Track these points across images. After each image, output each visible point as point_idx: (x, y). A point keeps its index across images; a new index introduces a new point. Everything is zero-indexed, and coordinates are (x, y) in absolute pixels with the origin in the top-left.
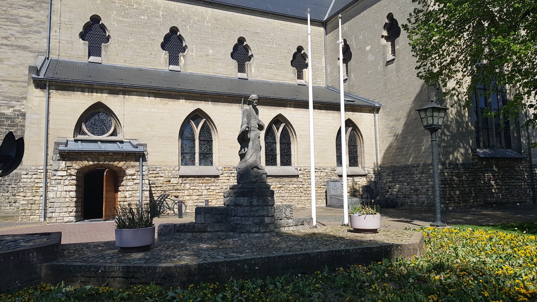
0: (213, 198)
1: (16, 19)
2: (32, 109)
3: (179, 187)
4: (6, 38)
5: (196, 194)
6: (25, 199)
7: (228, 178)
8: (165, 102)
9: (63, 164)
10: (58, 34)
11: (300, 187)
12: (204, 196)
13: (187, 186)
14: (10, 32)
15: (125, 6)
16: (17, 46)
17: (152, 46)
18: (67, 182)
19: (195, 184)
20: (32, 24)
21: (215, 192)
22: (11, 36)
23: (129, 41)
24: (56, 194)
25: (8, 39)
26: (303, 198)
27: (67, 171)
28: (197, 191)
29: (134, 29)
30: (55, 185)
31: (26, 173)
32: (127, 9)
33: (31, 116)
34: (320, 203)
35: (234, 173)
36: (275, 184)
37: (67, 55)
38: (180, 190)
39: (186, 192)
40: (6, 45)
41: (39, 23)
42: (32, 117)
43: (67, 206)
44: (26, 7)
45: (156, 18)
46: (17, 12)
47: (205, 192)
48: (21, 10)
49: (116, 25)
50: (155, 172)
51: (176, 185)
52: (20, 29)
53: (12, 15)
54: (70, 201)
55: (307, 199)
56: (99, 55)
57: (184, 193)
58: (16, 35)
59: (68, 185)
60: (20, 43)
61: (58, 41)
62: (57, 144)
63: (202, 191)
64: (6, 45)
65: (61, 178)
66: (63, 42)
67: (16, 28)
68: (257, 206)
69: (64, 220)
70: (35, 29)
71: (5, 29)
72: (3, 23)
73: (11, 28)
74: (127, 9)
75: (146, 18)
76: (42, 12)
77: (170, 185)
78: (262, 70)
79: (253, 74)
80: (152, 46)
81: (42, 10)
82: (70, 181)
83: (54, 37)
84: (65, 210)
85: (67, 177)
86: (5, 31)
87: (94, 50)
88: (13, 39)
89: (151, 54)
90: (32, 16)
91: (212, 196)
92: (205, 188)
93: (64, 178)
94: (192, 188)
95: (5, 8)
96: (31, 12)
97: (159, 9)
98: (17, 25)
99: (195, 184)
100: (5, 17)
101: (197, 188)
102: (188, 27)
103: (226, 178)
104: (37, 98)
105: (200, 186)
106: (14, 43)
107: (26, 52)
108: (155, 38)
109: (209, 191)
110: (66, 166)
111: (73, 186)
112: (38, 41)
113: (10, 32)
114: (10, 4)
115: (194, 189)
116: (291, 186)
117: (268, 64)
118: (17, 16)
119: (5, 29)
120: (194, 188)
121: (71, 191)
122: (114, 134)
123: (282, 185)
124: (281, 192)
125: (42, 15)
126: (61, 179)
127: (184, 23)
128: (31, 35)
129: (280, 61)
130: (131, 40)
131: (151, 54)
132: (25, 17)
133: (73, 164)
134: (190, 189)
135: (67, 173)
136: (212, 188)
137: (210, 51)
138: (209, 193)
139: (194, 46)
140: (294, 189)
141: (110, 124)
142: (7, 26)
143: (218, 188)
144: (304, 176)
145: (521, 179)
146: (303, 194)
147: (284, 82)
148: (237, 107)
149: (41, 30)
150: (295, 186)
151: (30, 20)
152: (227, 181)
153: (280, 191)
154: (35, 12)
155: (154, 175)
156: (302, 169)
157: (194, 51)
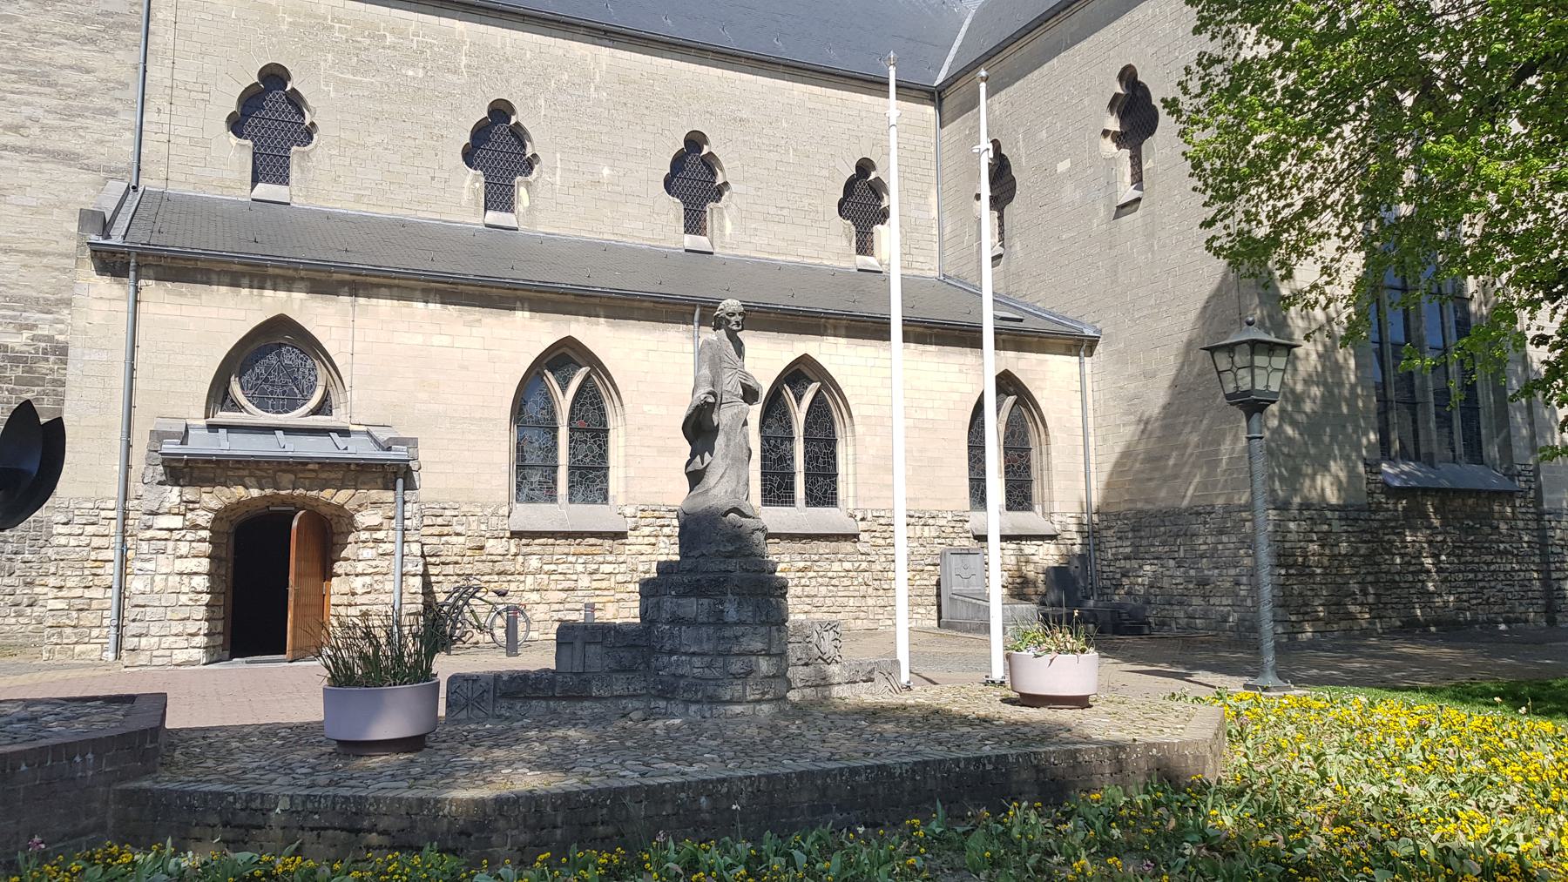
0: (609, 598)
1: (44, 74)
2: (86, 333)
3: (509, 567)
4: (16, 129)
5: (560, 587)
6: (60, 594)
7: (653, 540)
8: (471, 318)
9: (173, 495)
10: (165, 118)
11: (861, 568)
12: (580, 593)
13: (531, 562)
14: (27, 111)
15: (359, 39)
16: (47, 152)
17: (436, 155)
18: (184, 548)
19: (555, 557)
20: (92, 90)
21: (613, 580)
22: (28, 123)
23: (370, 141)
24: (153, 581)
25: (22, 131)
26: (870, 601)
27: (184, 515)
28: (561, 577)
29: (386, 107)
30: (149, 556)
31: (65, 520)
32: (366, 49)
33: (83, 354)
34: (919, 616)
35: (668, 526)
36: (787, 559)
37: (191, 179)
38: (512, 574)
39: (530, 579)
40: (15, 149)
41: (112, 85)
42: (86, 358)
43: (183, 617)
44: (75, 40)
45: (450, 76)
46: (49, 55)
47: (585, 581)
48: (59, 48)
49: (332, 95)
50: (440, 521)
51: (500, 558)
52: (55, 102)
53: (35, 63)
54: (191, 603)
55: (883, 604)
56: (283, 179)
57: (524, 582)
58: (45, 121)
59: (186, 557)
60: (56, 142)
61: (165, 138)
62: (159, 436)
63: (575, 577)
64: (15, 149)
65: (167, 537)
66: (179, 140)
67: (44, 101)
68: (736, 624)
69: (174, 657)
70: (98, 102)
71: (13, 104)
72: (9, 87)
73: (30, 99)
74: (366, 49)
75: (421, 74)
76: (120, 54)
77: (484, 558)
78: (753, 226)
79: (727, 240)
80: (436, 155)
81: (120, 49)
82: (194, 544)
83: (154, 128)
84: (177, 628)
85: (183, 532)
86: (14, 109)
87: (269, 166)
88: (36, 130)
89: (433, 178)
90: (90, 64)
91: (606, 593)
92: (583, 570)
93: (176, 535)
94: (546, 568)
95: (14, 43)
96: (88, 55)
97: (458, 50)
98: (48, 90)
99: (555, 557)
100: (13, 68)
101: (561, 568)
102: (542, 102)
103: (646, 540)
104: (100, 302)
105: (571, 563)
106: (39, 144)
107: (72, 169)
108: (445, 133)
109: (595, 577)
110: (182, 501)
111: (200, 560)
112: (107, 138)
113: (27, 111)
114: (29, 31)
115: (553, 572)
116: (836, 566)
117: (772, 210)
118: (49, 64)
119: (13, 104)
120: (553, 567)
121: (195, 573)
122: (323, 408)
123: (809, 563)
124: (808, 583)
125: (121, 63)
126: (166, 540)
127: (529, 91)
128: (88, 121)
129: (806, 201)
130: (377, 138)
131: (433, 178)
132: (71, 68)
133: (204, 495)
134: (540, 571)
135: (184, 520)
136: (607, 568)
137: (606, 171)
138: (595, 585)
139: (558, 155)
140: (843, 574)
141: (312, 379)
142: (21, 93)
143: (623, 568)
144: (874, 537)
145: (1512, 553)
146: (870, 590)
147: (817, 262)
148: (680, 335)
149: (118, 106)
150: (847, 565)
151: (86, 77)
152: (649, 549)
153: (803, 581)
154: (102, 55)
155: (436, 530)
156: (869, 517)
157: (558, 170)
